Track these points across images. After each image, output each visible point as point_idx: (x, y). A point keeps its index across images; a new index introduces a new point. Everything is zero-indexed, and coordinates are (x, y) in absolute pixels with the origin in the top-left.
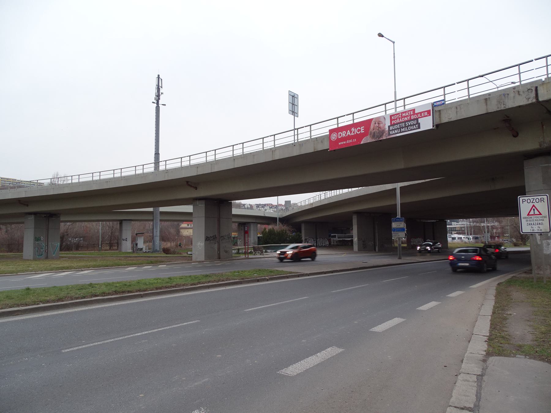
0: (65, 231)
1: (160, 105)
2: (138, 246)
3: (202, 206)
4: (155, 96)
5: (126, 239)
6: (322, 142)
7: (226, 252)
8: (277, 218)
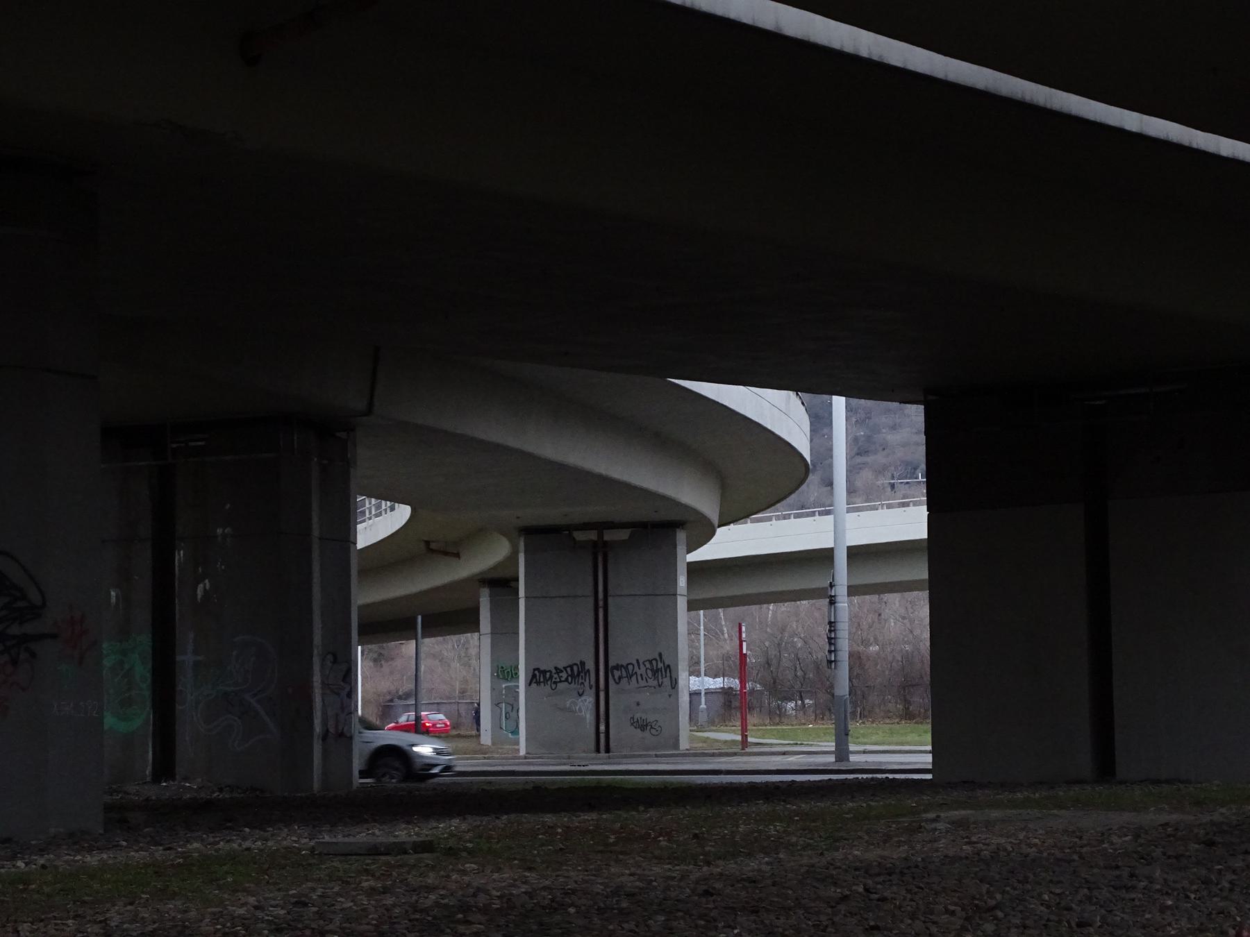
7: (643, 726)
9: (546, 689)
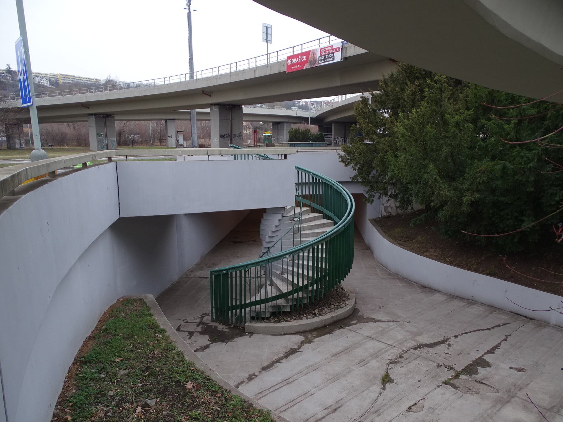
0: (122, 128)
1: (191, 11)
2: (179, 142)
3: (216, 110)
4: (186, 2)
5: (171, 136)
6: (283, 65)
8: (309, 117)
9: (222, 139)
